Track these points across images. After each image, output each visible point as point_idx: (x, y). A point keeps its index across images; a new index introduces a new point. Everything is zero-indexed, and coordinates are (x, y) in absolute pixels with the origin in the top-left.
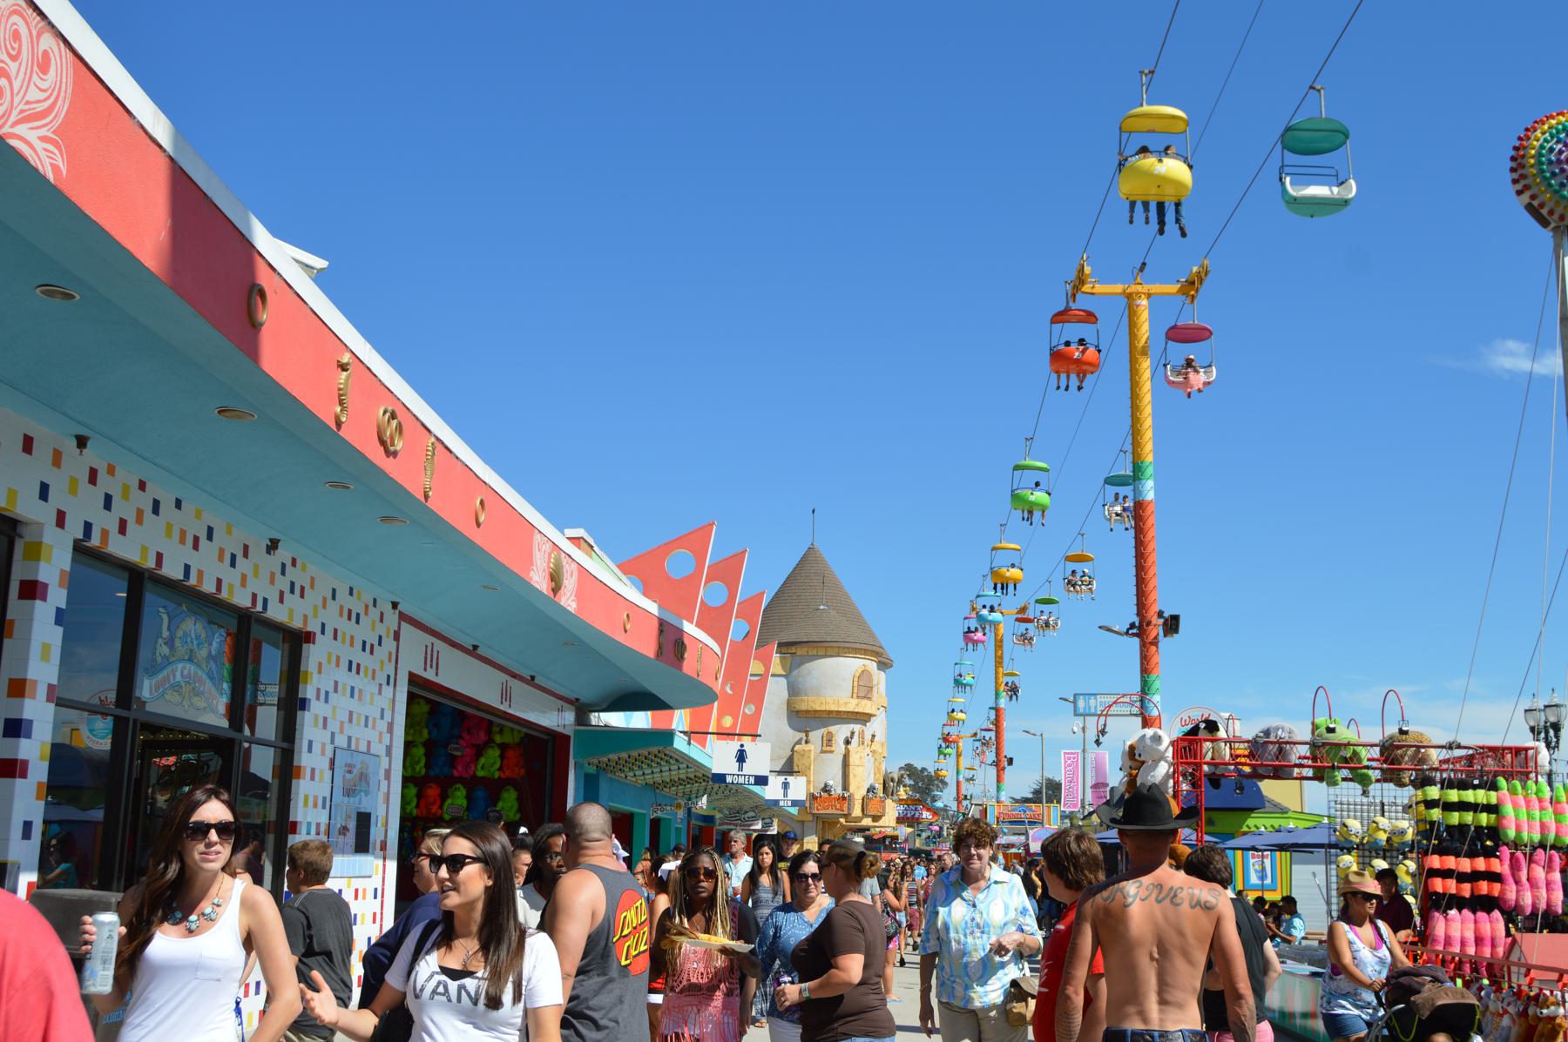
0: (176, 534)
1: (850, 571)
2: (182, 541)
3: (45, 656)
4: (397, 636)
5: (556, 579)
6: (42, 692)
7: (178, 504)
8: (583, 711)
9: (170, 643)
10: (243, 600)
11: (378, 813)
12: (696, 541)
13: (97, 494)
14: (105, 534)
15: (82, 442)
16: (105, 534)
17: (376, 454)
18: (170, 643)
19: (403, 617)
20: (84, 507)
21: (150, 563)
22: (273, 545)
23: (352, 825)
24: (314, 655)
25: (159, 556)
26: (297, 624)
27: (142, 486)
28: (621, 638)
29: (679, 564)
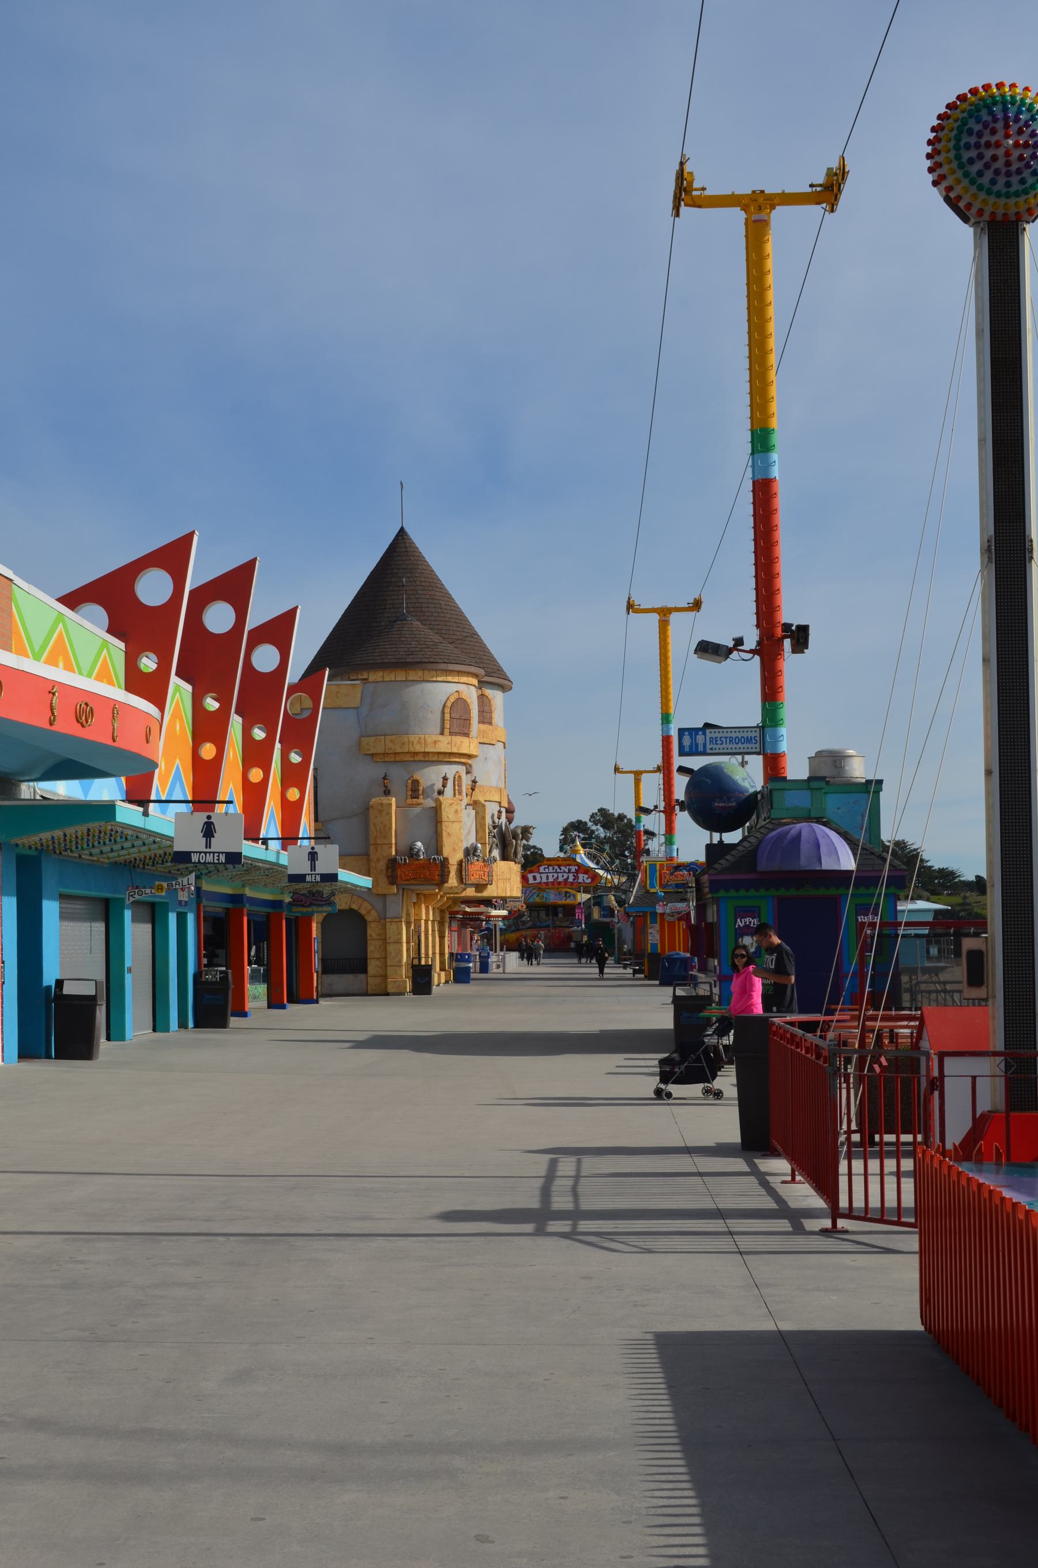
1: (455, 565)
12: (173, 557)
29: (153, 589)
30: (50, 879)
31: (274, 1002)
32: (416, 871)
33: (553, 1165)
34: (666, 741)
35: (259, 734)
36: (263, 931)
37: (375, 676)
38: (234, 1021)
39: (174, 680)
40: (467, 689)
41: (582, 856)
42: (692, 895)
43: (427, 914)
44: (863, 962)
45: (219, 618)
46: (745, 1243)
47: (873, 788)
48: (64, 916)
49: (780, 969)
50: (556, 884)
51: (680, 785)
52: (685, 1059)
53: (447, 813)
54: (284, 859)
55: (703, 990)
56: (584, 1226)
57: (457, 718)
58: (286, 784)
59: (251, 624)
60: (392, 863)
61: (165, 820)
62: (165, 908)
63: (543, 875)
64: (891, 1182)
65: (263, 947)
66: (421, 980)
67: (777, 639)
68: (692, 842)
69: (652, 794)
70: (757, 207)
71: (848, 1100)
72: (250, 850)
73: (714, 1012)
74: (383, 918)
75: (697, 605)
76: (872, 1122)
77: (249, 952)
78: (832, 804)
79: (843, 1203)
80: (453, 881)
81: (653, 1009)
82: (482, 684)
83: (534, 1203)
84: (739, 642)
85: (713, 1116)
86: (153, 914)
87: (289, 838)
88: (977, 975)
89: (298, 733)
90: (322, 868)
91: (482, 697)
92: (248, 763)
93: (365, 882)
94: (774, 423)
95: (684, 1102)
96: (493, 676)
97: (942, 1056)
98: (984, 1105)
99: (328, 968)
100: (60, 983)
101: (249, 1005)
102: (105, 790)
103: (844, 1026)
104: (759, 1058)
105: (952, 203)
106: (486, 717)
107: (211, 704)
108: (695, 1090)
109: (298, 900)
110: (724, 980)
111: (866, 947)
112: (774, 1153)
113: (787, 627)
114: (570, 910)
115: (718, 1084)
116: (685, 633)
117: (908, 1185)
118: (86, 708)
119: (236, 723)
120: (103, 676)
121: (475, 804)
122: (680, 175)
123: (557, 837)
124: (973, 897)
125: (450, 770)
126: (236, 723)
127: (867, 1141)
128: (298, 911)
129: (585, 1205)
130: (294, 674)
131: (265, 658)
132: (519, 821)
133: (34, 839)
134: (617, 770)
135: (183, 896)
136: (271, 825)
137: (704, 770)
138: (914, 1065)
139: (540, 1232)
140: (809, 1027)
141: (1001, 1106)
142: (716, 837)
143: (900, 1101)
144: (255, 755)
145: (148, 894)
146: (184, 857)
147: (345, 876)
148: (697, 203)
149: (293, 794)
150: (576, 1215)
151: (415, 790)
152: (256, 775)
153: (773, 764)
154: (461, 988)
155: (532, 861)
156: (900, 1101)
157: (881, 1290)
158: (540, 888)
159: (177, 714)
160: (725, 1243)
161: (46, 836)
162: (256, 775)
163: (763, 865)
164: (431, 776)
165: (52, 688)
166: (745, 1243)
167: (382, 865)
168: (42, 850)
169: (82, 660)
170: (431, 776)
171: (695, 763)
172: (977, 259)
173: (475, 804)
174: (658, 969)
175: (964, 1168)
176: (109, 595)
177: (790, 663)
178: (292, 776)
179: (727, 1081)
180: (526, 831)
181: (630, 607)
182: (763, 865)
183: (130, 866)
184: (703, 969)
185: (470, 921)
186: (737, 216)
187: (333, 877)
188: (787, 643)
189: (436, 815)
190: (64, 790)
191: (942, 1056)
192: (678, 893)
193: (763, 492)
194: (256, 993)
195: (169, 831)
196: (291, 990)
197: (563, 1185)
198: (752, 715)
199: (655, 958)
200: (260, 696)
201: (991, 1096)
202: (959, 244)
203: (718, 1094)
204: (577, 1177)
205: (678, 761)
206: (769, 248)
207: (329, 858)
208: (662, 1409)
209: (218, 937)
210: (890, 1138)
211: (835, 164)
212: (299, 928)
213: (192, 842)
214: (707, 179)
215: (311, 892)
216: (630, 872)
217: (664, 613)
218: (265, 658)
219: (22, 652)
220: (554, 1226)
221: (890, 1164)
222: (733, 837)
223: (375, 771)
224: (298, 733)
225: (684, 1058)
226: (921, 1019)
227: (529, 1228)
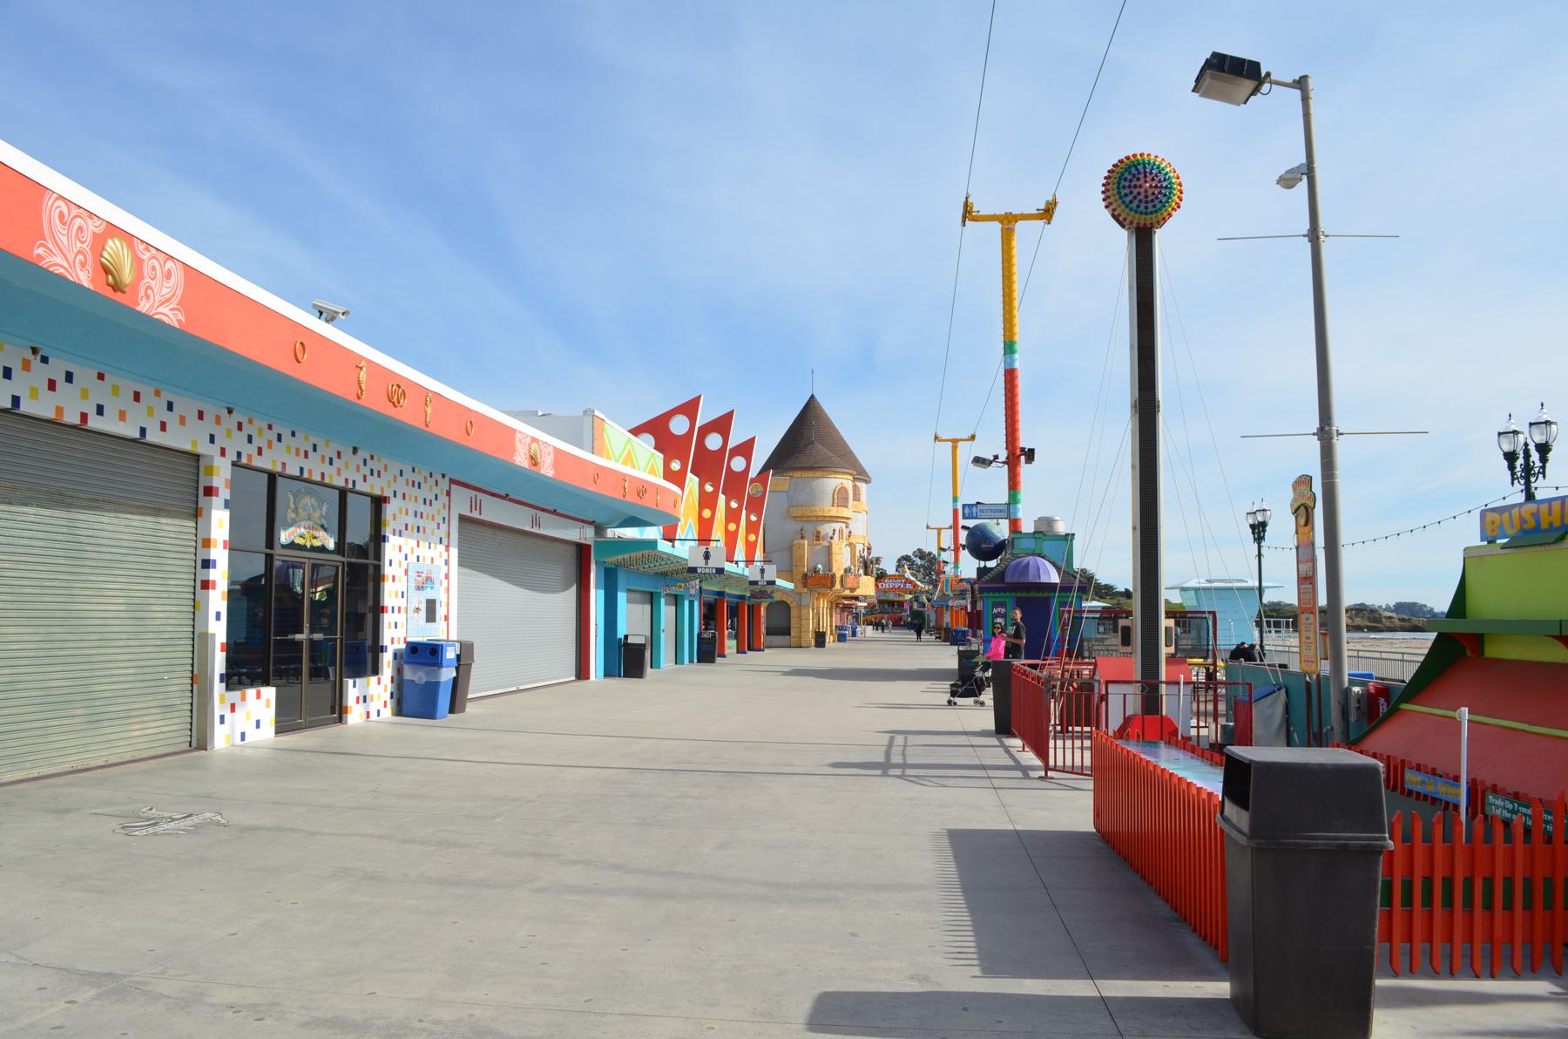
0: (293, 451)
1: (841, 416)
2: (297, 453)
3: (221, 526)
4: (448, 493)
5: (534, 460)
6: (221, 544)
7: (293, 434)
8: (599, 529)
9: (296, 511)
10: (340, 483)
11: (441, 597)
12: (690, 409)
13: (243, 436)
14: (250, 457)
15: (230, 411)
16: (250, 457)
17: (388, 410)
18: (296, 511)
19: (452, 481)
20: (236, 443)
21: (279, 469)
22: (355, 450)
23: (423, 607)
24: (389, 510)
25: (284, 464)
26: (377, 492)
27: (270, 427)
28: (592, 488)
29: (679, 426)
30: (622, 579)
31: (740, 651)
32: (816, 581)
33: (892, 739)
34: (955, 512)
35: (734, 505)
36: (734, 612)
37: (797, 474)
38: (718, 660)
39: (690, 476)
40: (846, 482)
41: (908, 574)
42: (969, 596)
43: (823, 604)
44: (1063, 631)
45: (713, 442)
46: (997, 783)
47: (1069, 538)
48: (629, 601)
49: (1017, 635)
50: (894, 589)
51: (963, 535)
52: (965, 684)
53: (835, 549)
54: (747, 572)
55: (974, 647)
56: (909, 772)
57: (841, 498)
58: (748, 532)
59: (731, 445)
60: (805, 576)
61: (685, 550)
62: (683, 597)
63: (887, 584)
64: (1078, 753)
65: (734, 620)
66: (820, 640)
67: (1017, 456)
68: (969, 567)
69: (947, 540)
70: (1008, 221)
71: (1054, 708)
72: (729, 567)
73: (980, 659)
74: (799, 606)
75: (973, 438)
76: (1067, 720)
77: (727, 623)
78: (1047, 547)
79: (1051, 763)
80: (838, 586)
81: (947, 657)
82: (855, 479)
83: (882, 759)
84: (996, 457)
85: (980, 714)
86: (676, 600)
87: (749, 561)
88: (1126, 641)
89: (755, 505)
90: (768, 577)
91: (855, 487)
92: (728, 520)
93: (790, 586)
94: (1017, 338)
95: (963, 707)
96: (861, 475)
97: (1107, 683)
98: (1129, 712)
99: (769, 633)
100: (626, 637)
101: (727, 652)
102: (652, 533)
103: (1053, 669)
104: (1004, 682)
105: (1116, 217)
106: (857, 498)
107: (709, 488)
108: (970, 701)
109: (753, 596)
110: (986, 642)
111: (1065, 624)
112: (1013, 735)
113: (1022, 449)
114: (901, 604)
115: (982, 698)
116: (966, 452)
117: (1087, 754)
118: (643, 488)
119: (722, 498)
120: (652, 472)
121: (850, 545)
122: (966, 204)
123: (895, 564)
124: (1123, 600)
125: (837, 526)
126: (722, 498)
127: (1064, 731)
128: (753, 601)
129: (909, 761)
130: (753, 473)
131: (738, 464)
132: (874, 555)
133: (614, 559)
134: (968, 213)
135: (692, 592)
136: (740, 554)
137: (976, 527)
138: (1092, 689)
139: (885, 774)
140: (1034, 667)
141: (1139, 712)
142: (982, 564)
143: (1083, 709)
144: (732, 516)
145: (674, 590)
146: (693, 570)
147: (780, 582)
148: (975, 219)
149: (752, 537)
150: (904, 766)
151: (818, 537)
152: (732, 527)
153: (1014, 525)
154: (842, 645)
155: (881, 576)
156: (1083, 709)
157: (1071, 809)
158: (885, 591)
159: (690, 493)
160: (986, 783)
161: (620, 557)
162: (732, 527)
163: (1008, 579)
164: (826, 529)
165: (624, 477)
166: (997, 783)
167: (799, 577)
168: (618, 565)
169: (641, 462)
170: (826, 529)
171: (971, 523)
172: (1129, 248)
173: (850, 545)
174: (950, 636)
175: (1119, 742)
176: (656, 429)
177: (1024, 469)
178: (752, 528)
179: (988, 696)
180: (878, 560)
181: (936, 438)
182: (1008, 579)
183: (665, 574)
184: (974, 636)
185: (846, 608)
186: (997, 226)
187: (773, 583)
188: (1023, 458)
189: (829, 549)
190: (630, 533)
191: (1107, 683)
192: (962, 595)
193: (1010, 376)
194: (730, 645)
195: (686, 556)
196: (749, 644)
197: (896, 750)
198: (1002, 497)
199: (948, 630)
200: (735, 484)
201: (1134, 706)
202: (1120, 241)
203: (982, 704)
204: (905, 746)
205: (962, 522)
206: (1015, 243)
207: (771, 572)
208: (951, 869)
209: (711, 614)
210: (1078, 729)
211: (1050, 198)
212: (753, 611)
213: (698, 562)
214: (980, 207)
215: (761, 591)
216: (935, 584)
217: (955, 442)
218: (738, 464)
219: (608, 458)
220: (892, 772)
221: (1078, 743)
222: (992, 564)
223: (798, 526)
224: (755, 505)
225: (964, 683)
226: (1095, 664)
227: (879, 772)
